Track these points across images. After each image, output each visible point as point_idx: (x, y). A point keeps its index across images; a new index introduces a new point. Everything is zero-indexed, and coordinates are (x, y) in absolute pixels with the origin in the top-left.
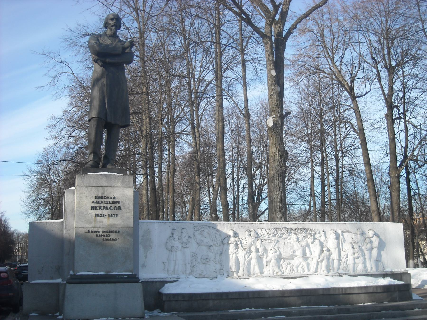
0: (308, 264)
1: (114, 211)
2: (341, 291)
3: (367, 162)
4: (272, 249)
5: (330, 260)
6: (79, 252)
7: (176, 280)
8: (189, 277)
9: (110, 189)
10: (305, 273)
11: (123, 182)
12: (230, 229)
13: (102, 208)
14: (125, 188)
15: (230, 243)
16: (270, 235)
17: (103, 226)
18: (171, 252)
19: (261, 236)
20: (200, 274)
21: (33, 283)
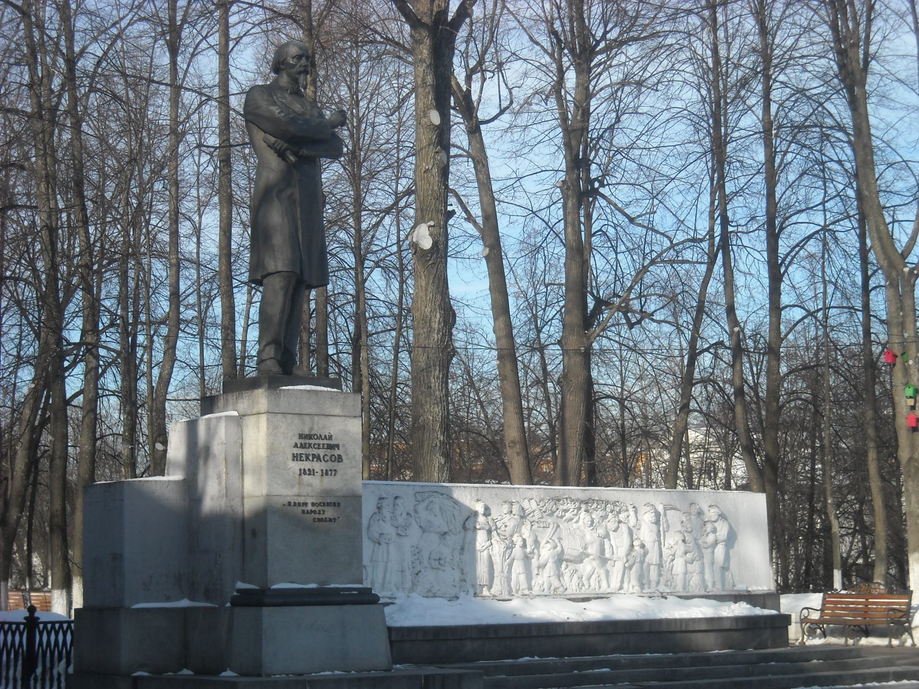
0: (607, 572)
1: (330, 463)
2: (679, 625)
3: (402, 282)
5: (645, 565)
6: (276, 543)
7: (390, 601)
9: (323, 421)
10: (602, 591)
12: (475, 498)
13: (311, 458)
15: (478, 527)
18: (377, 545)
20: (429, 591)
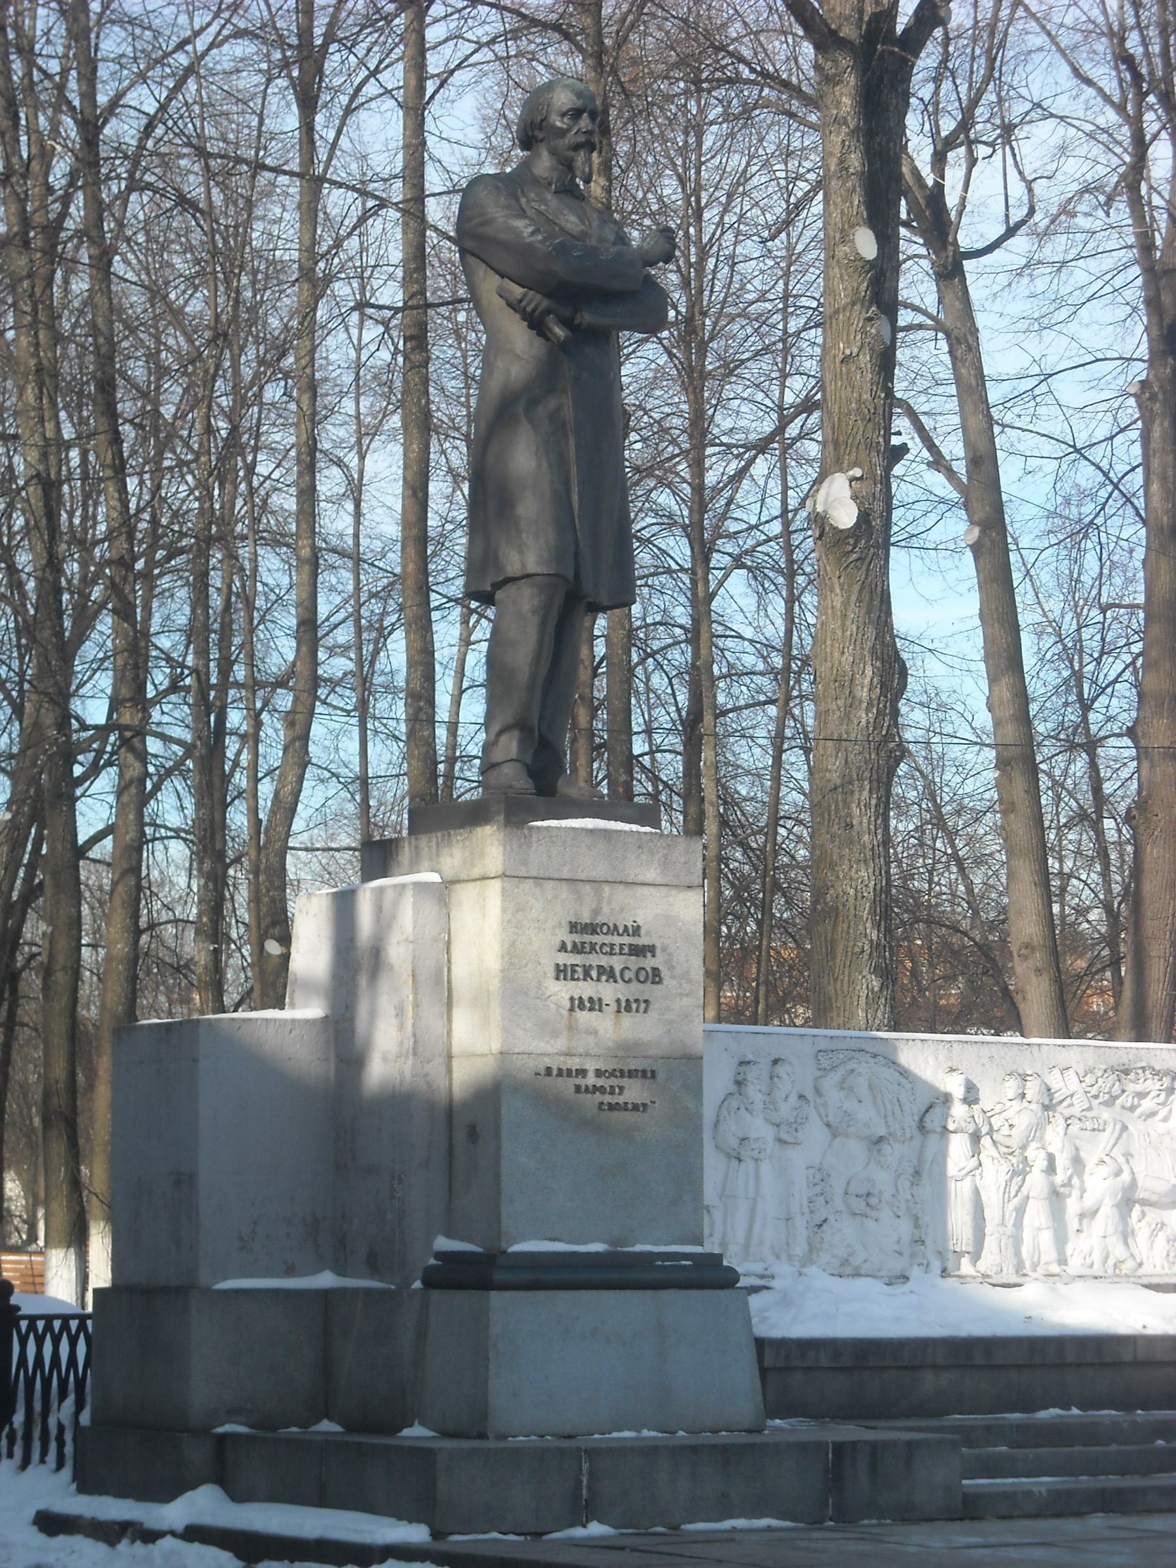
1: (635, 985)
3: (792, 600)
4: (1107, 1159)
8: (804, 1270)
11: (666, 864)
13: (594, 974)
14: (674, 892)
15: (951, 1127)
16: (1096, 1097)
17: (597, 1051)
18: (734, 1163)
19: (1062, 1102)
20: (845, 1262)
21: (227, 1293)
